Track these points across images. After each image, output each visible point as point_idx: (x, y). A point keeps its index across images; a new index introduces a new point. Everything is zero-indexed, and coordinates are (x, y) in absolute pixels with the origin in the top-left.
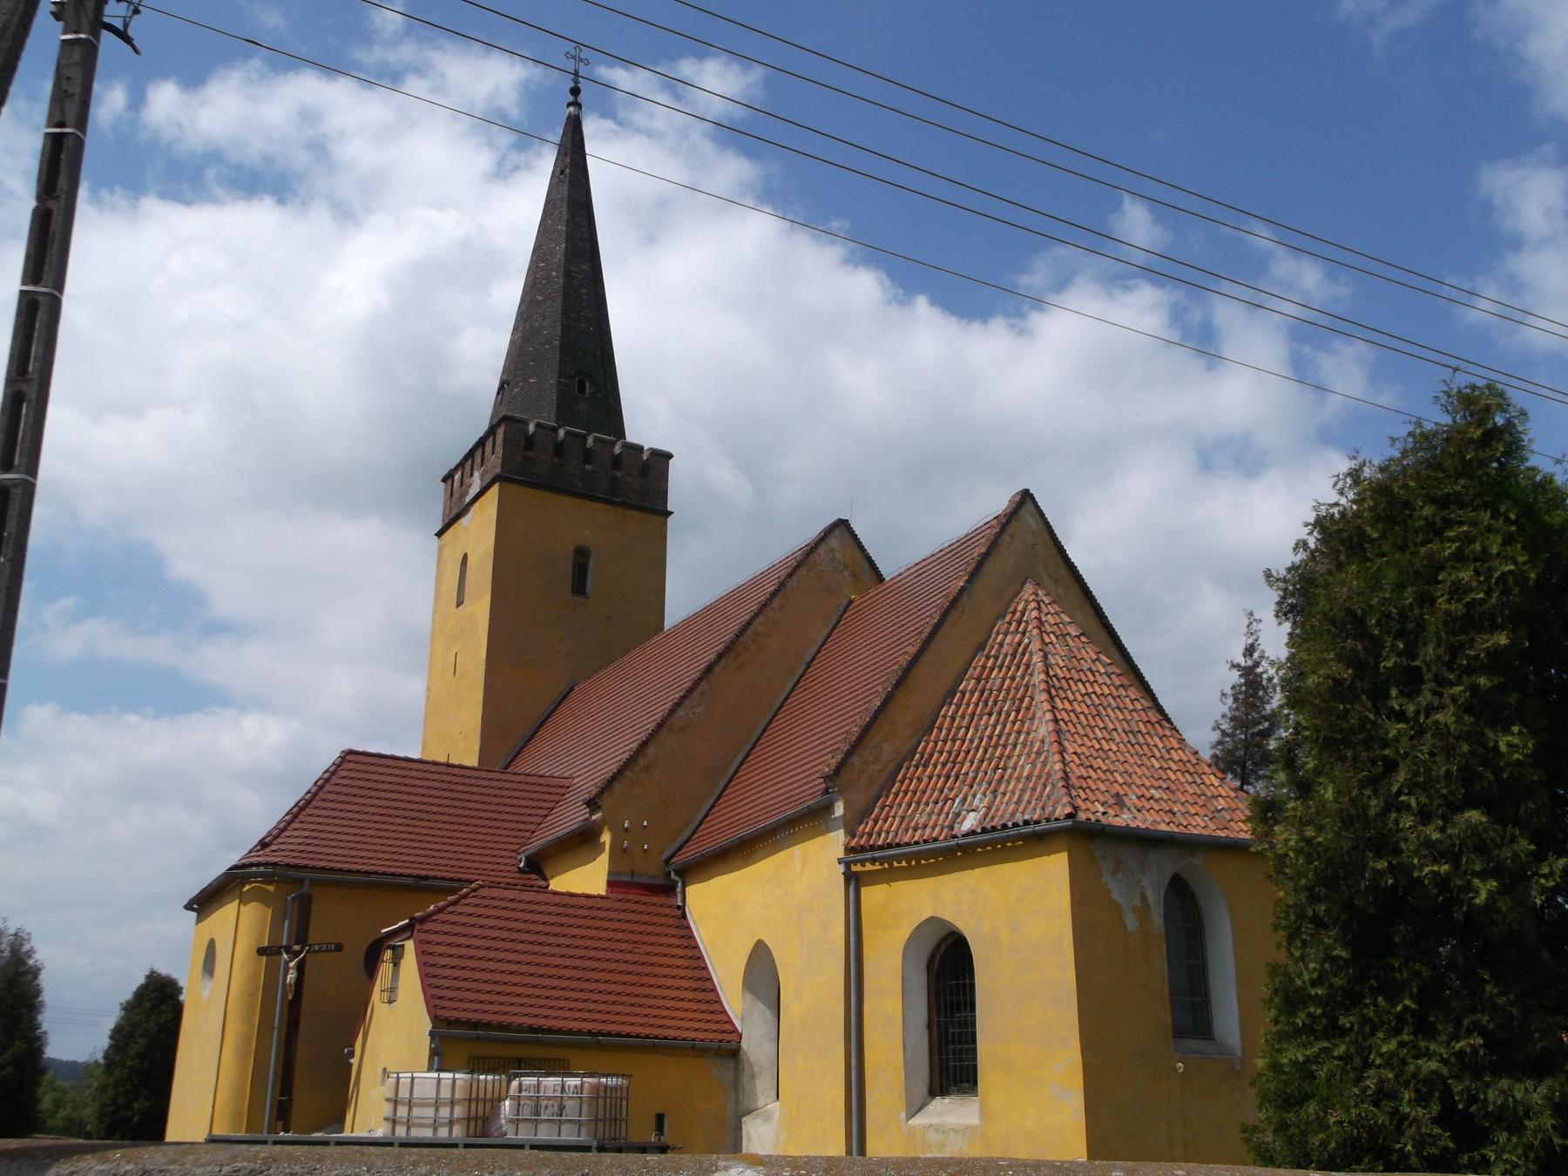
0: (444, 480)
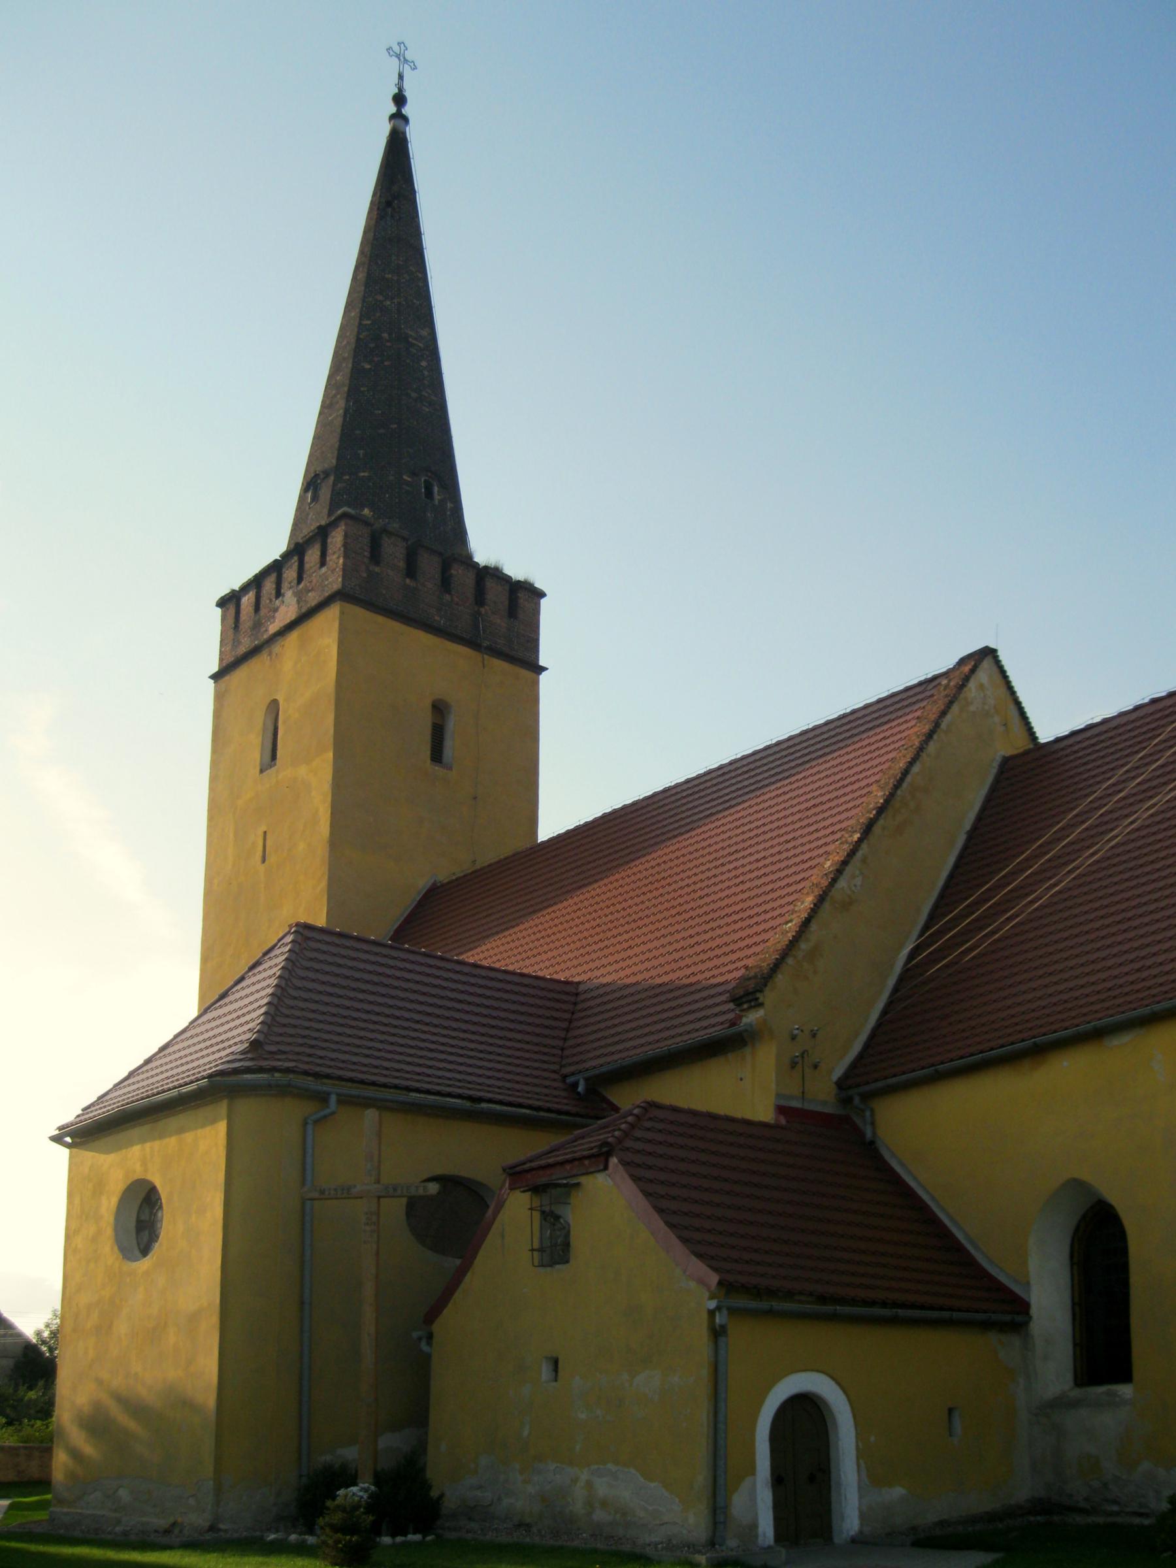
0: (222, 603)
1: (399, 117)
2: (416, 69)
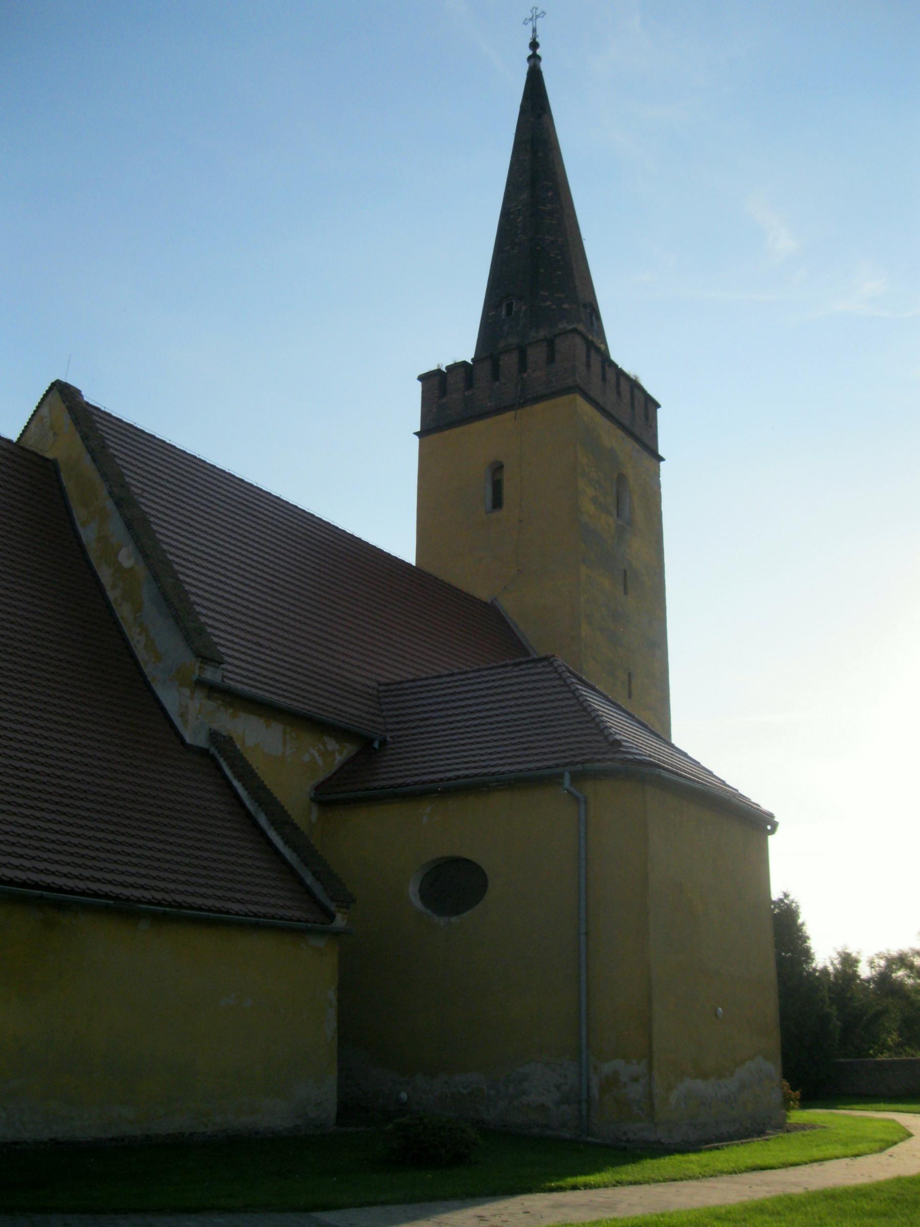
1: (534, 59)
2: (523, 23)
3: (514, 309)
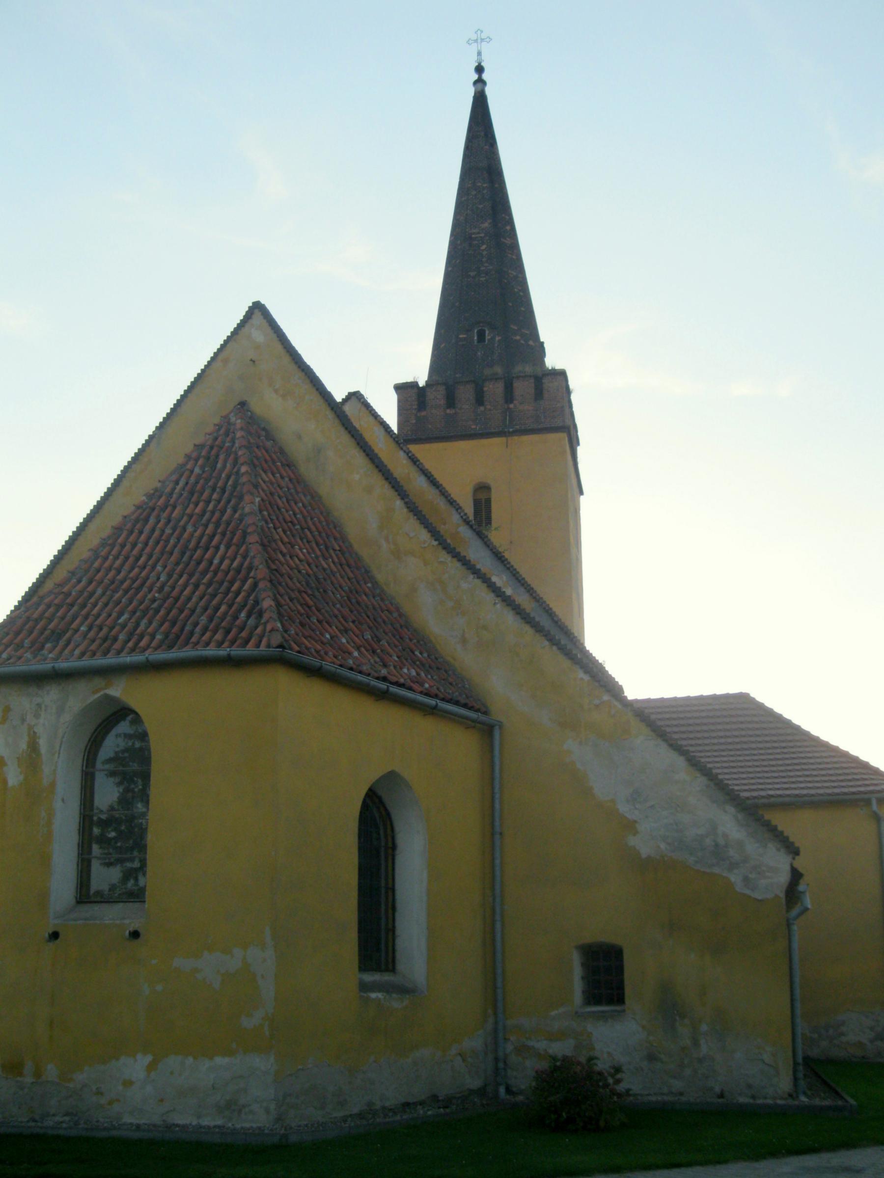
1: (480, 82)
2: (467, 42)
3: (487, 337)
